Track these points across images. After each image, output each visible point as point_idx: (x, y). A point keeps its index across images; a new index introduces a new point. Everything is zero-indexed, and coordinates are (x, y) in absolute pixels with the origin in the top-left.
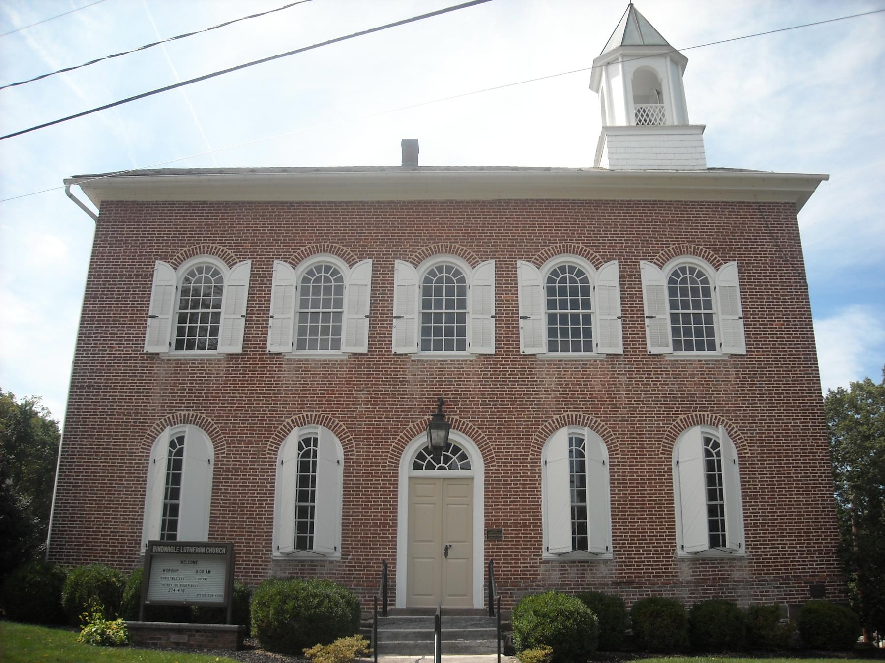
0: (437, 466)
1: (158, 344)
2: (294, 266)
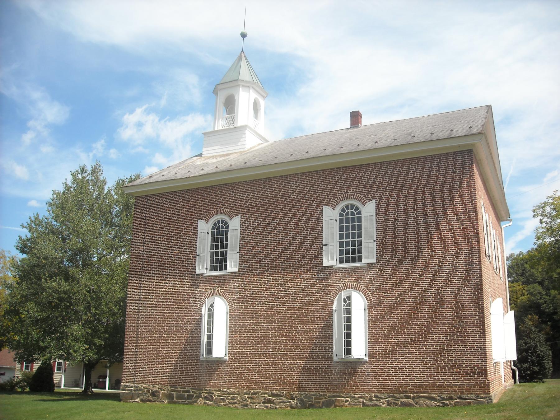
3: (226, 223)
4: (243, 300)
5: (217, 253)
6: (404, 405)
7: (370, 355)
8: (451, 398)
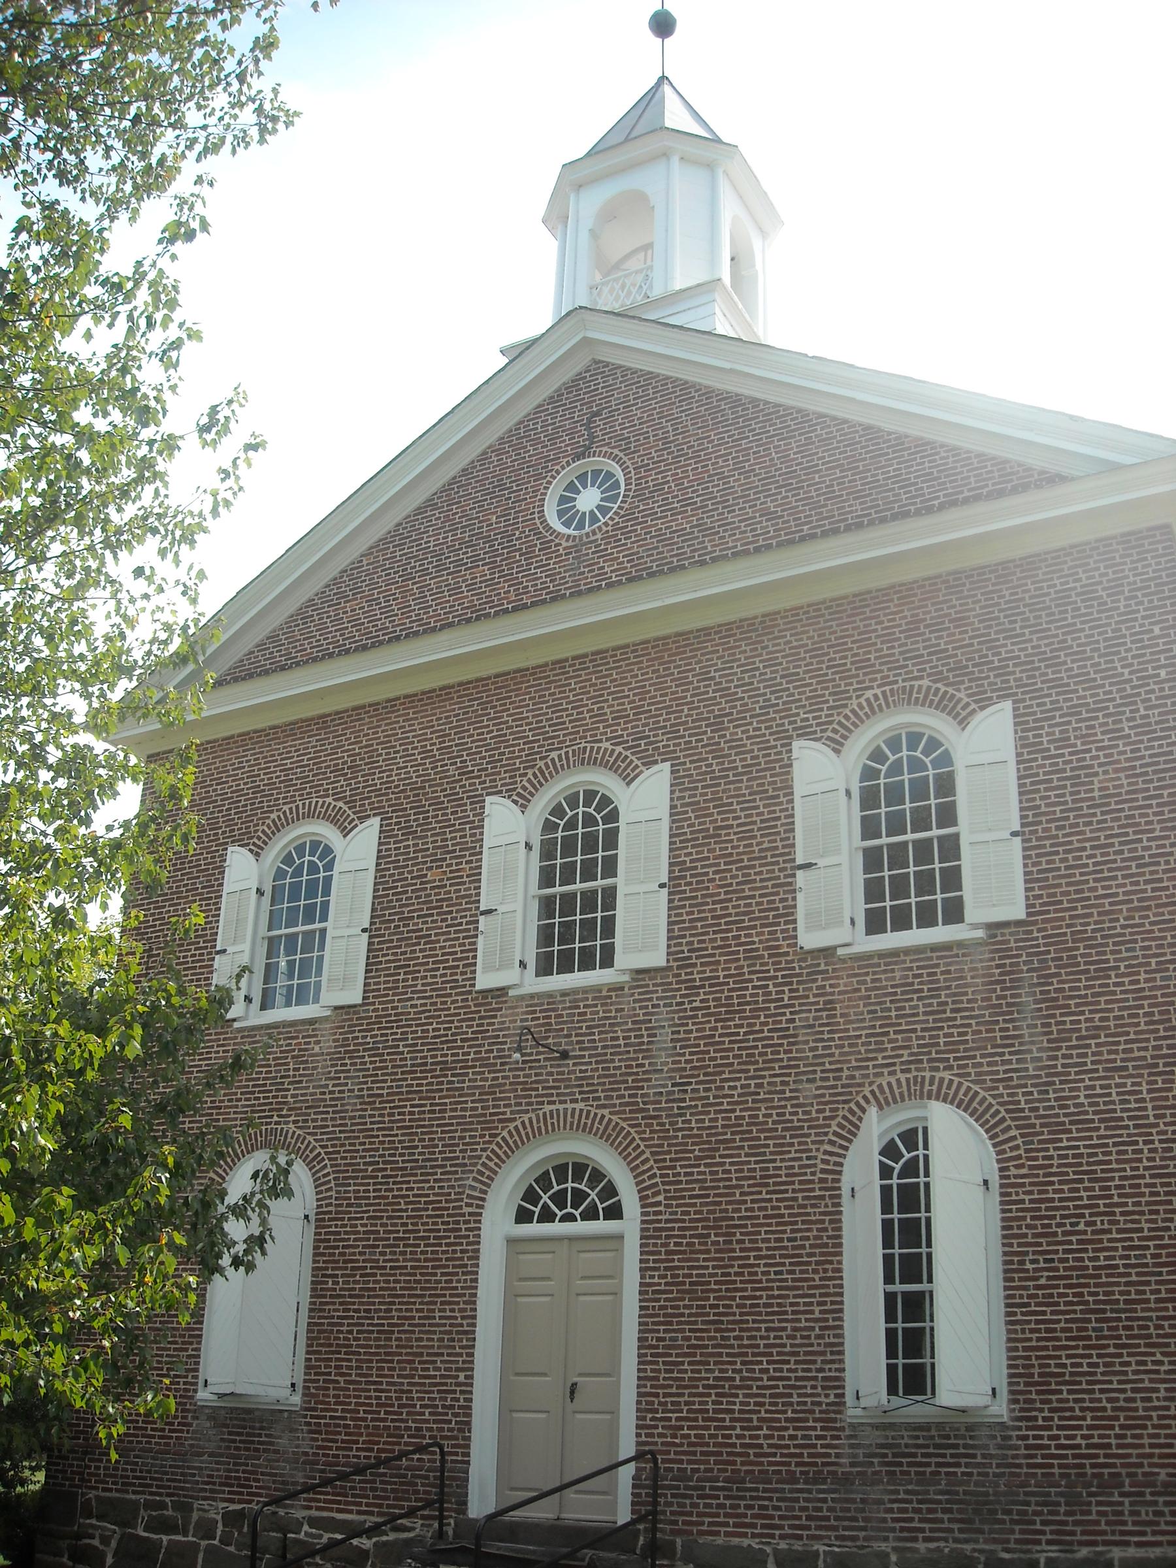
0: (560, 1214)
1: (503, 966)
2: (837, 747)
3: (328, 850)
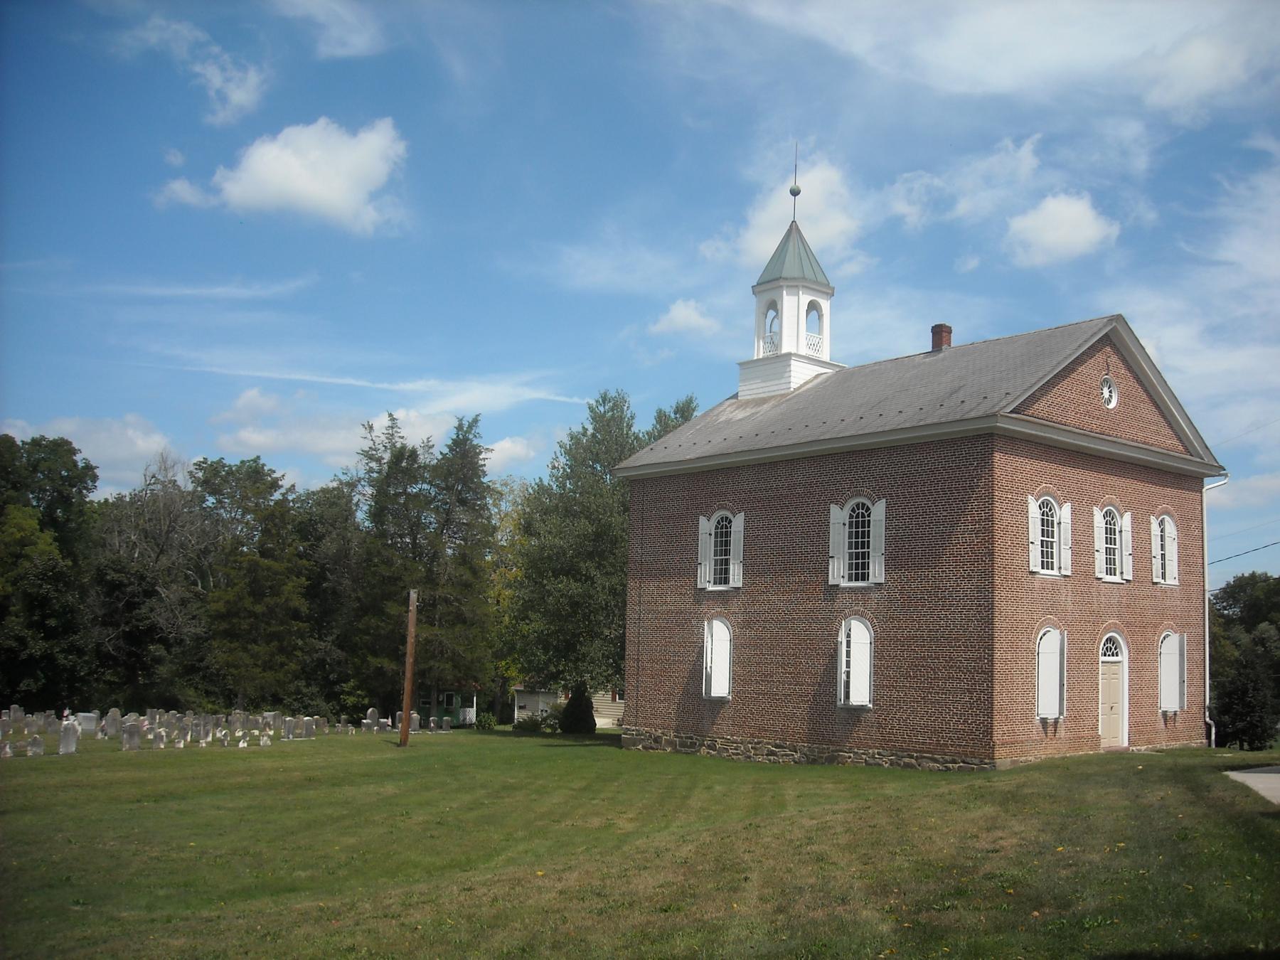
3: (868, 509)
4: (747, 624)
5: (857, 554)
6: (907, 766)
7: (874, 700)
8: (954, 762)
